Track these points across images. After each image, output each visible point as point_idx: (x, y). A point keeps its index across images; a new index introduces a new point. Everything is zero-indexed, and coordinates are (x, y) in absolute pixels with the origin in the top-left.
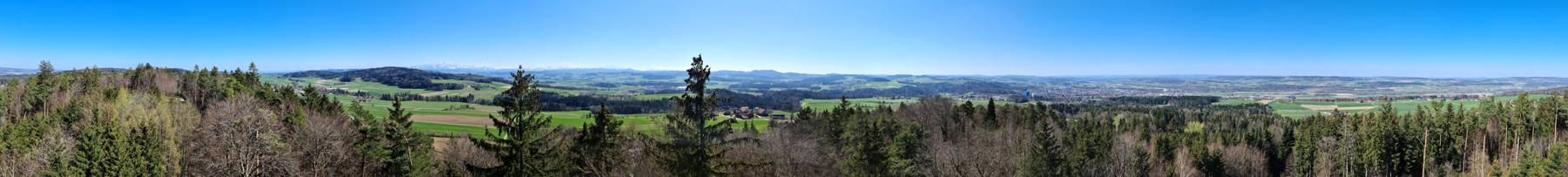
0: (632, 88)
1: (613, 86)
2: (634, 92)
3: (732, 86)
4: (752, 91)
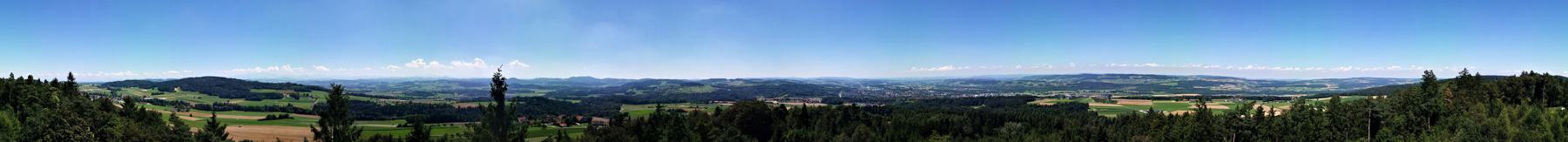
0: (449, 96)
1: (429, 94)
2: (450, 100)
3: (550, 94)
4: (570, 99)
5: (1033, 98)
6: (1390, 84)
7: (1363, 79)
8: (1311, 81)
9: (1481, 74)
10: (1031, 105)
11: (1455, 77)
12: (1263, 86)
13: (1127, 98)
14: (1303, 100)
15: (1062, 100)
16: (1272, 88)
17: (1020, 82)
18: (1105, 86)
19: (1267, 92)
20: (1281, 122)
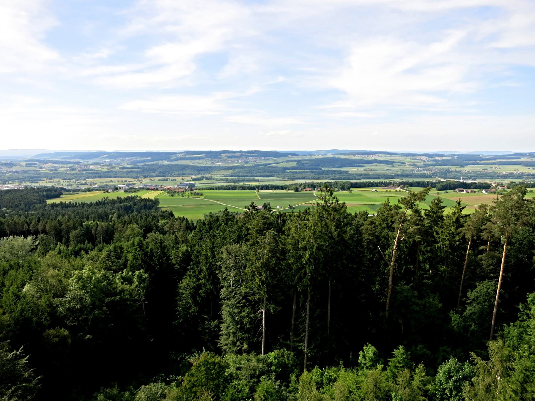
5: (56, 193)
10: (54, 205)
12: (437, 163)
13: (219, 188)
15: (113, 196)
16: (453, 168)
17: (30, 163)
18: (182, 170)
19: (444, 174)
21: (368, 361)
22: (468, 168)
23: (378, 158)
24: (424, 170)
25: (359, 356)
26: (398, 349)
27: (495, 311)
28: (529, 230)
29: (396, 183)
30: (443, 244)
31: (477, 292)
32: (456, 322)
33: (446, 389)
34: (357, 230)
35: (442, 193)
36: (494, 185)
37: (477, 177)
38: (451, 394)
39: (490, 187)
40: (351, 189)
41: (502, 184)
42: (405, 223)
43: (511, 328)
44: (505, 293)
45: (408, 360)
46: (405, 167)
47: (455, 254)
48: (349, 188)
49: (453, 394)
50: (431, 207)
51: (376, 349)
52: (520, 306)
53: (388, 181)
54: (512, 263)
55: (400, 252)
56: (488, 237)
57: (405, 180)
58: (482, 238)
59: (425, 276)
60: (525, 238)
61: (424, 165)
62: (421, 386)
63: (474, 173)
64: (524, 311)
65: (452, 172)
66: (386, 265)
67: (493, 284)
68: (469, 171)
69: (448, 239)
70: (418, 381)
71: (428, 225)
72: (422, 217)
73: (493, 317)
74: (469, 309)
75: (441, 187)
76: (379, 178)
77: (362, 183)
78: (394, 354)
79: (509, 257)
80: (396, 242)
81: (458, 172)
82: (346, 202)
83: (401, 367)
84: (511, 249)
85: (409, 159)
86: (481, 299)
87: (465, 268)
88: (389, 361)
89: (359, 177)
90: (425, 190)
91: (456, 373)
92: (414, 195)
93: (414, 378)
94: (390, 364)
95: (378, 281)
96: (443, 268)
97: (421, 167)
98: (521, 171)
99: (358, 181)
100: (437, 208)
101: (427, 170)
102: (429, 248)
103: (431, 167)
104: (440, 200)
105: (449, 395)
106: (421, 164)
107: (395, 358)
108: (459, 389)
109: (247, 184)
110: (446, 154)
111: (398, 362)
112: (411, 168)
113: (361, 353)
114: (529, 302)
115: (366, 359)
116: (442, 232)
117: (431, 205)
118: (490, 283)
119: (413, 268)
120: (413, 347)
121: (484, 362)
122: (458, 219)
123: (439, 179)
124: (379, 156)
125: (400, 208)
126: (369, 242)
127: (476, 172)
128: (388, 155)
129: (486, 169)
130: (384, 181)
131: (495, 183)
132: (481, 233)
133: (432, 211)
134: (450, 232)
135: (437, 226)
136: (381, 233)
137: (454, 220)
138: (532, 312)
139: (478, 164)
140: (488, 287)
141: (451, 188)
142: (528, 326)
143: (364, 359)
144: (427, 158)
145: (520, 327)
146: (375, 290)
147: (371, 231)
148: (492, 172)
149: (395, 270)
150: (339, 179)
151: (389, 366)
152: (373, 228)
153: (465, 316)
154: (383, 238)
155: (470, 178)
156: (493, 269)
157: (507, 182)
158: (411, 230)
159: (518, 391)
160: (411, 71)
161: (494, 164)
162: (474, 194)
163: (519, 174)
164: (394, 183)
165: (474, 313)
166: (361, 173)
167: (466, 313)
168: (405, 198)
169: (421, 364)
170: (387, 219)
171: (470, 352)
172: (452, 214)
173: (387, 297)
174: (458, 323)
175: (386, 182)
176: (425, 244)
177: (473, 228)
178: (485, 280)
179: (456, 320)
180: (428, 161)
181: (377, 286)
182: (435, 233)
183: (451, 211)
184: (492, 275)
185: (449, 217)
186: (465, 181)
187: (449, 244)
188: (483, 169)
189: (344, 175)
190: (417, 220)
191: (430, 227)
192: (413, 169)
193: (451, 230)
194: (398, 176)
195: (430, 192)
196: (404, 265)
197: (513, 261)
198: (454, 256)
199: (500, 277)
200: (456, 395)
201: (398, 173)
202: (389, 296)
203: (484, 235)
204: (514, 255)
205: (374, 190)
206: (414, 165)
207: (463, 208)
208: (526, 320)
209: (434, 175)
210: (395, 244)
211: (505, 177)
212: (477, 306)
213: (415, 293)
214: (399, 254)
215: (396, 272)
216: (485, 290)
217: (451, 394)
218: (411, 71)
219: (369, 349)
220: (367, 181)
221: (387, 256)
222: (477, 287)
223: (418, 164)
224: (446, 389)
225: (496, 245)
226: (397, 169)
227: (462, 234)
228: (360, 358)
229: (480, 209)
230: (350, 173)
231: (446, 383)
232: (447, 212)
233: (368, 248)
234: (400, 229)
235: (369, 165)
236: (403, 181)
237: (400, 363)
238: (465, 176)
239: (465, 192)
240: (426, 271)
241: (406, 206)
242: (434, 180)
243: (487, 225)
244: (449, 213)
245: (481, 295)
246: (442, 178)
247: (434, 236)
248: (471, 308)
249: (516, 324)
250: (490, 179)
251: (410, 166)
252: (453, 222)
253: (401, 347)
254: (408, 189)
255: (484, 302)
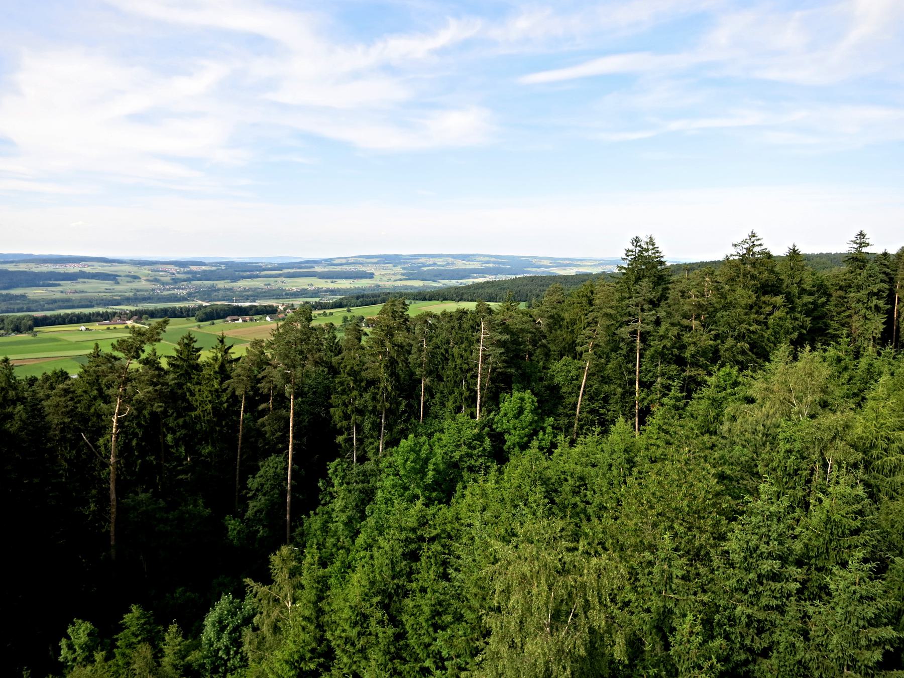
6: (533, 272)
7: (464, 257)
8: (329, 262)
9: (805, 249)
11: (720, 257)
12: (195, 276)
14: (306, 314)
16: (221, 284)
19: (207, 294)
20: (86, 378)
21: (79, 651)
22: (243, 284)
23: (87, 269)
24: (173, 289)
25: (60, 649)
26: (130, 611)
27: (288, 500)
28: (323, 371)
29: (126, 314)
30: (202, 411)
31: (262, 476)
32: (235, 532)
33: (219, 649)
34: (33, 410)
35: (205, 326)
36: (281, 308)
37: (257, 296)
38: (228, 654)
39: (277, 311)
40: (36, 329)
41: (292, 305)
42: (129, 384)
43: (313, 518)
44: (300, 469)
45: (150, 625)
46: (140, 284)
47: (224, 423)
48: (30, 329)
49: (232, 652)
50: (177, 351)
51: (93, 625)
52: (320, 484)
53: (109, 311)
54: (305, 423)
55: (126, 437)
56: (270, 388)
57: (141, 307)
58: (260, 392)
59: (179, 468)
60: (320, 383)
61: (173, 279)
62: (177, 662)
63: (252, 291)
64: (325, 490)
65: (219, 290)
66: (105, 465)
67: (282, 459)
68: (245, 288)
69: (210, 401)
70: (172, 656)
71: (173, 382)
72: (162, 369)
73: (288, 508)
74: (253, 507)
75: (204, 316)
76: (92, 306)
77: (59, 316)
78: (124, 624)
79: (301, 415)
80: (114, 421)
81: (230, 289)
82: (10, 357)
83: (139, 642)
84: (302, 402)
85: (145, 270)
86: (267, 487)
87: (240, 443)
88: (117, 640)
89: (51, 306)
90: (159, 323)
91: (232, 618)
92: (140, 333)
93: (164, 652)
94: (118, 644)
95: (94, 496)
96: (207, 450)
97: (167, 284)
98: (317, 286)
99: (48, 313)
100: (189, 351)
101: (178, 289)
102: (181, 421)
103: (185, 283)
104: (191, 339)
105: (226, 658)
106: (168, 279)
107: (126, 631)
108: (237, 643)
109: (461, 283)
110: (207, 261)
111: (133, 634)
112: (150, 286)
113: (63, 643)
114: (330, 476)
115: (75, 651)
116: (200, 390)
117: (178, 347)
118: (277, 459)
119: (155, 459)
120: (168, 595)
121: (265, 589)
122: (222, 366)
123: (200, 302)
124: (88, 266)
125: (116, 359)
126: (65, 428)
127: (256, 289)
128: (105, 264)
129: (269, 285)
130: (101, 310)
131: (283, 304)
132: (259, 385)
133: (179, 358)
134: (213, 389)
135: (191, 383)
136: (89, 407)
137: (217, 369)
138: (335, 489)
139: (257, 277)
140: (275, 465)
141: (219, 317)
142: (333, 510)
143: (71, 652)
144: (177, 268)
145: (323, 514)
146: (88, 515)
147: (67, 406)
148: (278, 289)
149: (121, 470)
150: (7, 312)
151: (118, 647)
152: (71, 400)
153: (247, 519)
154: (93, 416)
155: (247, 299)
156: (280, 436)
157: (299, 303)
158: (140, 395)
159: (313, 617)
160: (139, 118)
161: (280, 276)
162: (254, 323)
163: (314, 290)
164: (121, 314)
165: (260, 511)
166: (54, 297)
167: (250, 513)
168: (124, 341)
169: (172, 624)
170: (98, 380)
171: (244, 580)
172: (213, 360)
173: (110, 522)
174: (239, 532)
175: (107, 312)
176: (175, 414)
177: (245, 378)
178: (271, 456)
179: (235, 529)
180: (178, 273)
181: (92, 505)
182: (188, 394)
183: (211, 355)
184: (280, 446)
185: (209, 365)
186: (240, 304)
187: (213, 408)
188: (265, 285)
189: (19, 304)
190: (153, 376)
191: (180, 385)
192: (153, 286)
193: (213, 386)
194: (127, 301)
195: (168, 328)
196: (138, 457)
197: (307, 420)
198: (222, 427)
199: (290, 447)
200: (236, 653)
201: (127, 294)
202: (113, 520)
203: (264, 387)
204: (308, 411)
205: (83, 328)
206: (156, 280)
207: (230, 348)
208: (330, 502)
209: (190, 297)
210: (115, 424)
211: (296, 295)
212: (263, 499)
213: (160, 503)
214: (124, 442)
215: (122, 473)
216: (272, 470)
217: (228, 654)
218: (139, 118)
219: (79, 629)
220: (69, 311)
221: (102, 448)
222: (260, 470)
223: (162, 278)
224: (219, 649)
225: (281, 400)
226: (124, 288)
227: (230, 389)
228: (62, 652)
229: (253, 347)
230: (32, 298)
231: (219, 641)
232: (205, 356)
233: (63, 439)
234: (121, 396)
235: (69, 282)
236: (137, 308)
237: (137, 636)
238: (240, 296)
239: (240, 321)
240: (180, 460)
241: (126, 355)
242: (191, 305)
243: (266, 371)
244: (208, 358)
245: (267, 480)
246: (203, 300)
247: (188, 399)
248: (255, 503)
249: (317, 511)
250: (276, 299)
251: (149, 283)
252: (215, 372)
253: (134, 608)
254: (147, 323)
255: (273, 489)
